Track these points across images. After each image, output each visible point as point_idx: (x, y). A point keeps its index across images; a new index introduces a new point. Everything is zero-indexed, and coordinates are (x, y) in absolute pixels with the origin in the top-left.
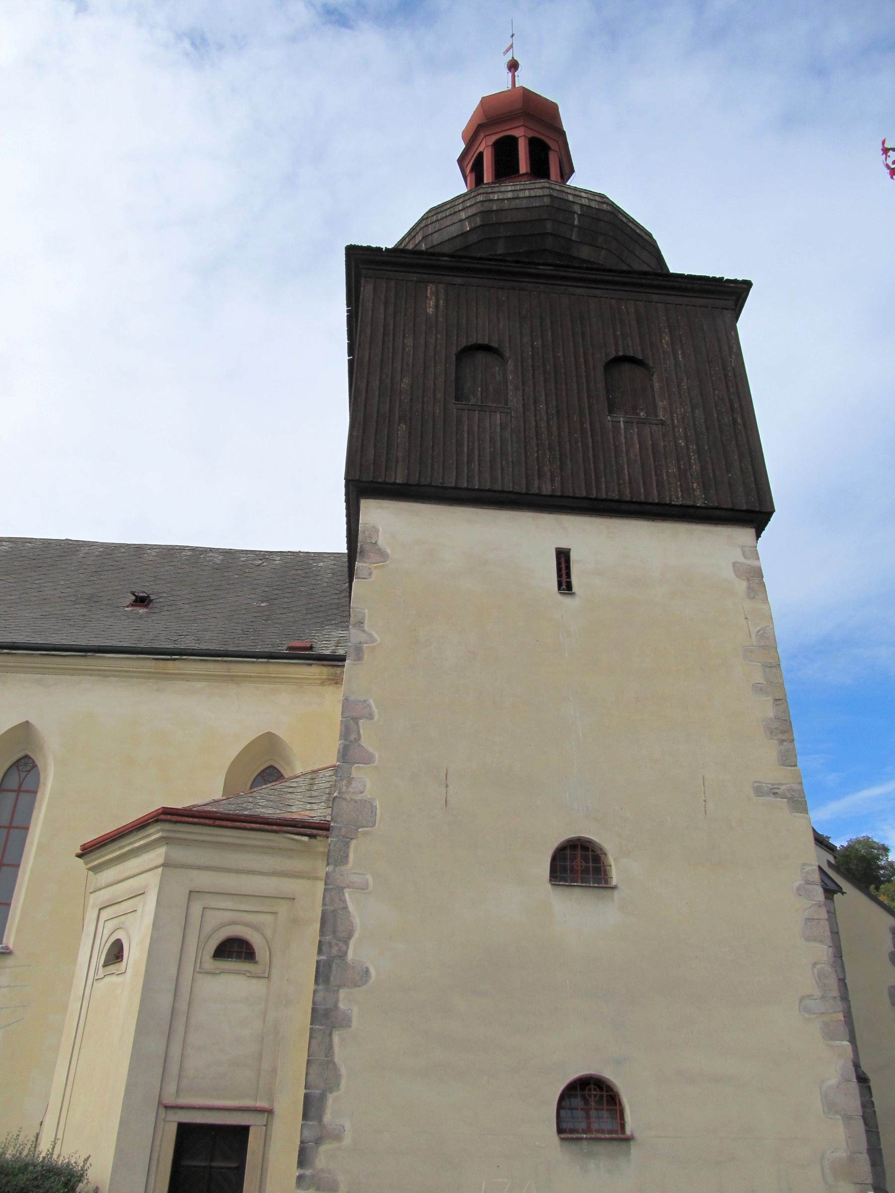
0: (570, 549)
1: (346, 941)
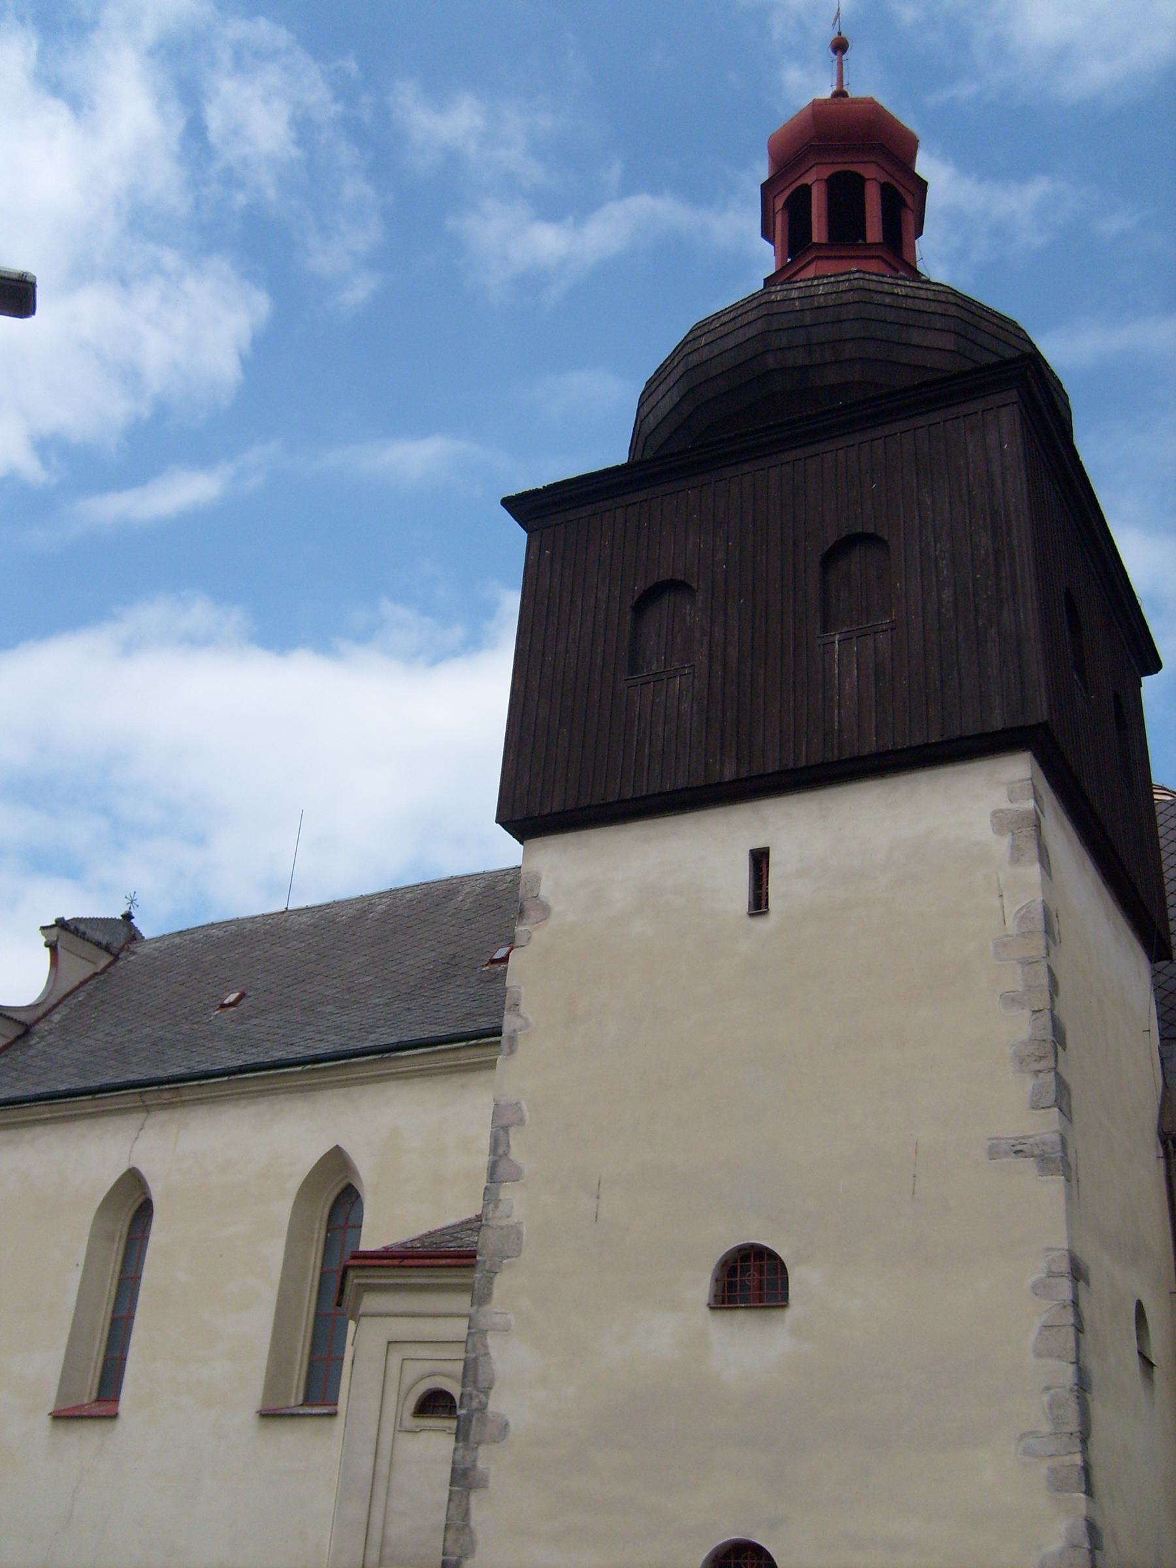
0: (769, 847)
1: (486, 1391)
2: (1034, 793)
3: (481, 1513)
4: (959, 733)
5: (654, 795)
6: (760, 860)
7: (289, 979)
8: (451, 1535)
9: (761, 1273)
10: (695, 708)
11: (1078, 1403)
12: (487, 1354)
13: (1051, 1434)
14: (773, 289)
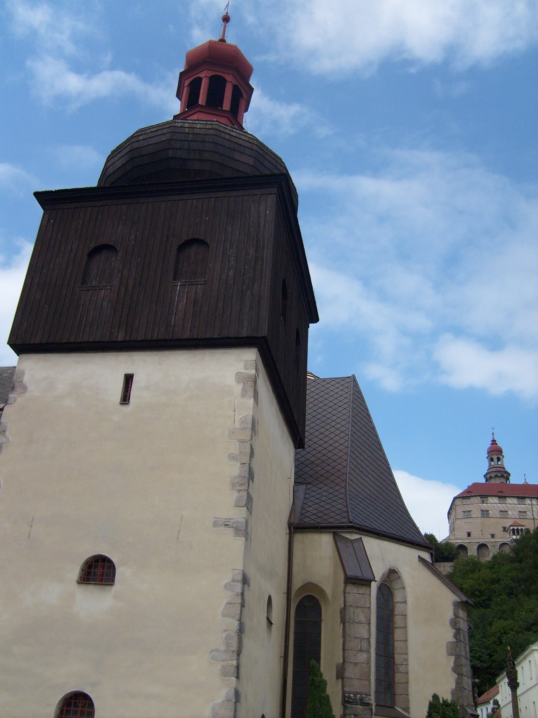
2: (256, 367)
4: (227, 335)
5: (84, 342)
6: (129, 379)
9: (103, 569)
10: (110, 305)
11: (238, 638)
13: (225, 651)
14: (177, 121)
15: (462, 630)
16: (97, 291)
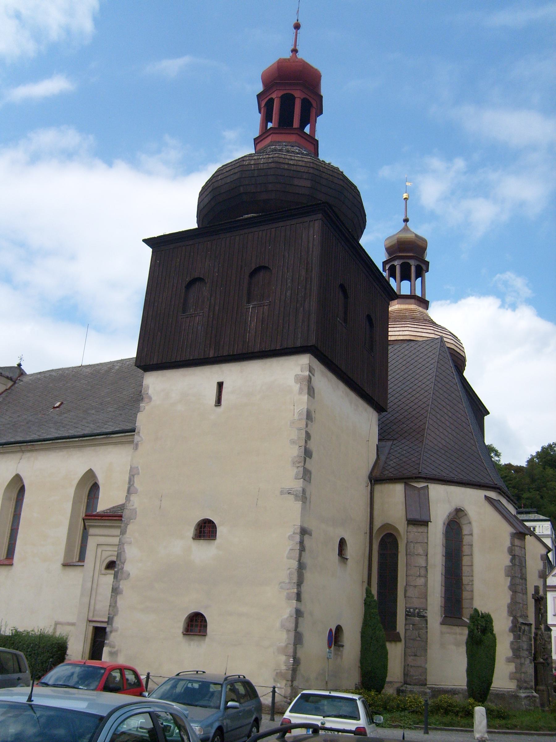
1: (123, 563)
3: (120, 602)
6: (220, 385)
7: (80, 397)
8: (111, 609)
12: (124, 551)
15: (517, 556)
16: (194, 318)
